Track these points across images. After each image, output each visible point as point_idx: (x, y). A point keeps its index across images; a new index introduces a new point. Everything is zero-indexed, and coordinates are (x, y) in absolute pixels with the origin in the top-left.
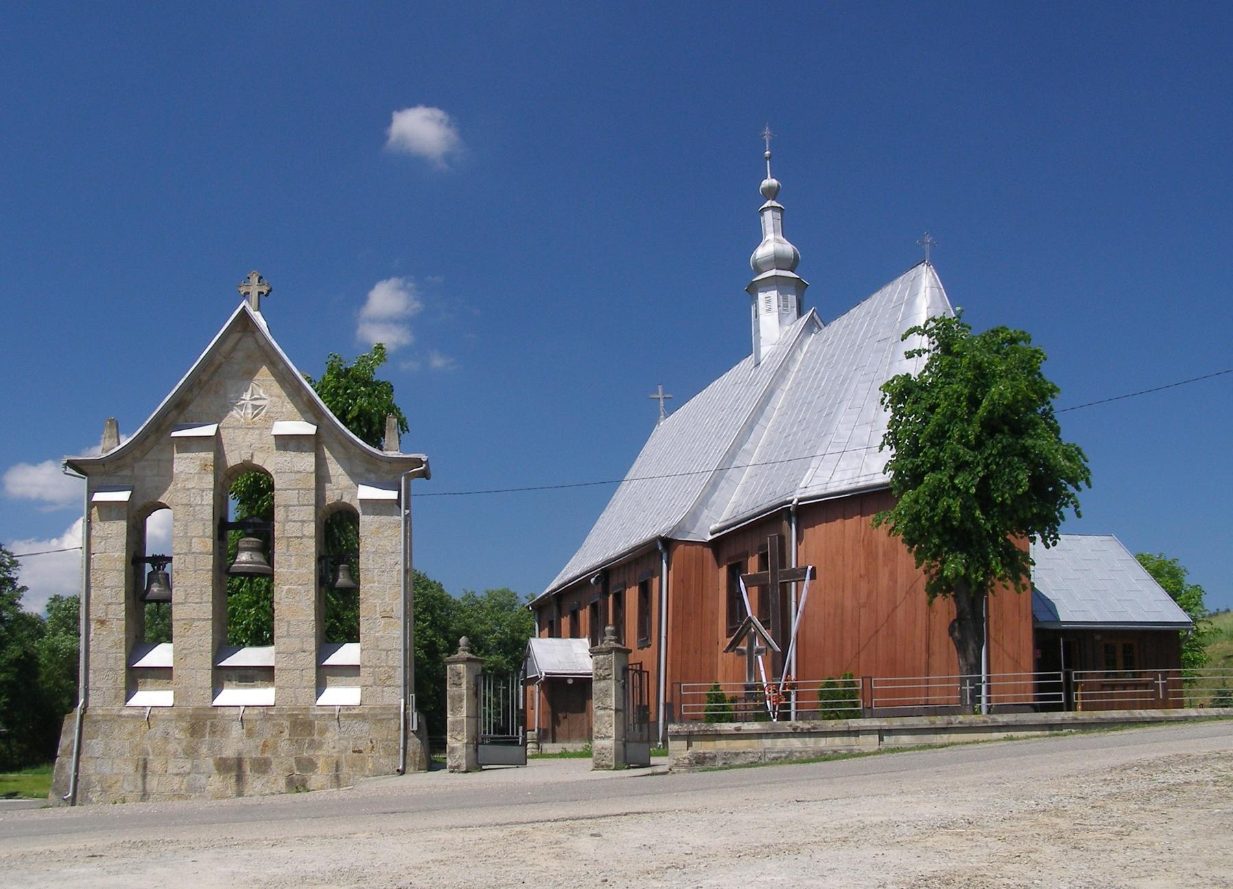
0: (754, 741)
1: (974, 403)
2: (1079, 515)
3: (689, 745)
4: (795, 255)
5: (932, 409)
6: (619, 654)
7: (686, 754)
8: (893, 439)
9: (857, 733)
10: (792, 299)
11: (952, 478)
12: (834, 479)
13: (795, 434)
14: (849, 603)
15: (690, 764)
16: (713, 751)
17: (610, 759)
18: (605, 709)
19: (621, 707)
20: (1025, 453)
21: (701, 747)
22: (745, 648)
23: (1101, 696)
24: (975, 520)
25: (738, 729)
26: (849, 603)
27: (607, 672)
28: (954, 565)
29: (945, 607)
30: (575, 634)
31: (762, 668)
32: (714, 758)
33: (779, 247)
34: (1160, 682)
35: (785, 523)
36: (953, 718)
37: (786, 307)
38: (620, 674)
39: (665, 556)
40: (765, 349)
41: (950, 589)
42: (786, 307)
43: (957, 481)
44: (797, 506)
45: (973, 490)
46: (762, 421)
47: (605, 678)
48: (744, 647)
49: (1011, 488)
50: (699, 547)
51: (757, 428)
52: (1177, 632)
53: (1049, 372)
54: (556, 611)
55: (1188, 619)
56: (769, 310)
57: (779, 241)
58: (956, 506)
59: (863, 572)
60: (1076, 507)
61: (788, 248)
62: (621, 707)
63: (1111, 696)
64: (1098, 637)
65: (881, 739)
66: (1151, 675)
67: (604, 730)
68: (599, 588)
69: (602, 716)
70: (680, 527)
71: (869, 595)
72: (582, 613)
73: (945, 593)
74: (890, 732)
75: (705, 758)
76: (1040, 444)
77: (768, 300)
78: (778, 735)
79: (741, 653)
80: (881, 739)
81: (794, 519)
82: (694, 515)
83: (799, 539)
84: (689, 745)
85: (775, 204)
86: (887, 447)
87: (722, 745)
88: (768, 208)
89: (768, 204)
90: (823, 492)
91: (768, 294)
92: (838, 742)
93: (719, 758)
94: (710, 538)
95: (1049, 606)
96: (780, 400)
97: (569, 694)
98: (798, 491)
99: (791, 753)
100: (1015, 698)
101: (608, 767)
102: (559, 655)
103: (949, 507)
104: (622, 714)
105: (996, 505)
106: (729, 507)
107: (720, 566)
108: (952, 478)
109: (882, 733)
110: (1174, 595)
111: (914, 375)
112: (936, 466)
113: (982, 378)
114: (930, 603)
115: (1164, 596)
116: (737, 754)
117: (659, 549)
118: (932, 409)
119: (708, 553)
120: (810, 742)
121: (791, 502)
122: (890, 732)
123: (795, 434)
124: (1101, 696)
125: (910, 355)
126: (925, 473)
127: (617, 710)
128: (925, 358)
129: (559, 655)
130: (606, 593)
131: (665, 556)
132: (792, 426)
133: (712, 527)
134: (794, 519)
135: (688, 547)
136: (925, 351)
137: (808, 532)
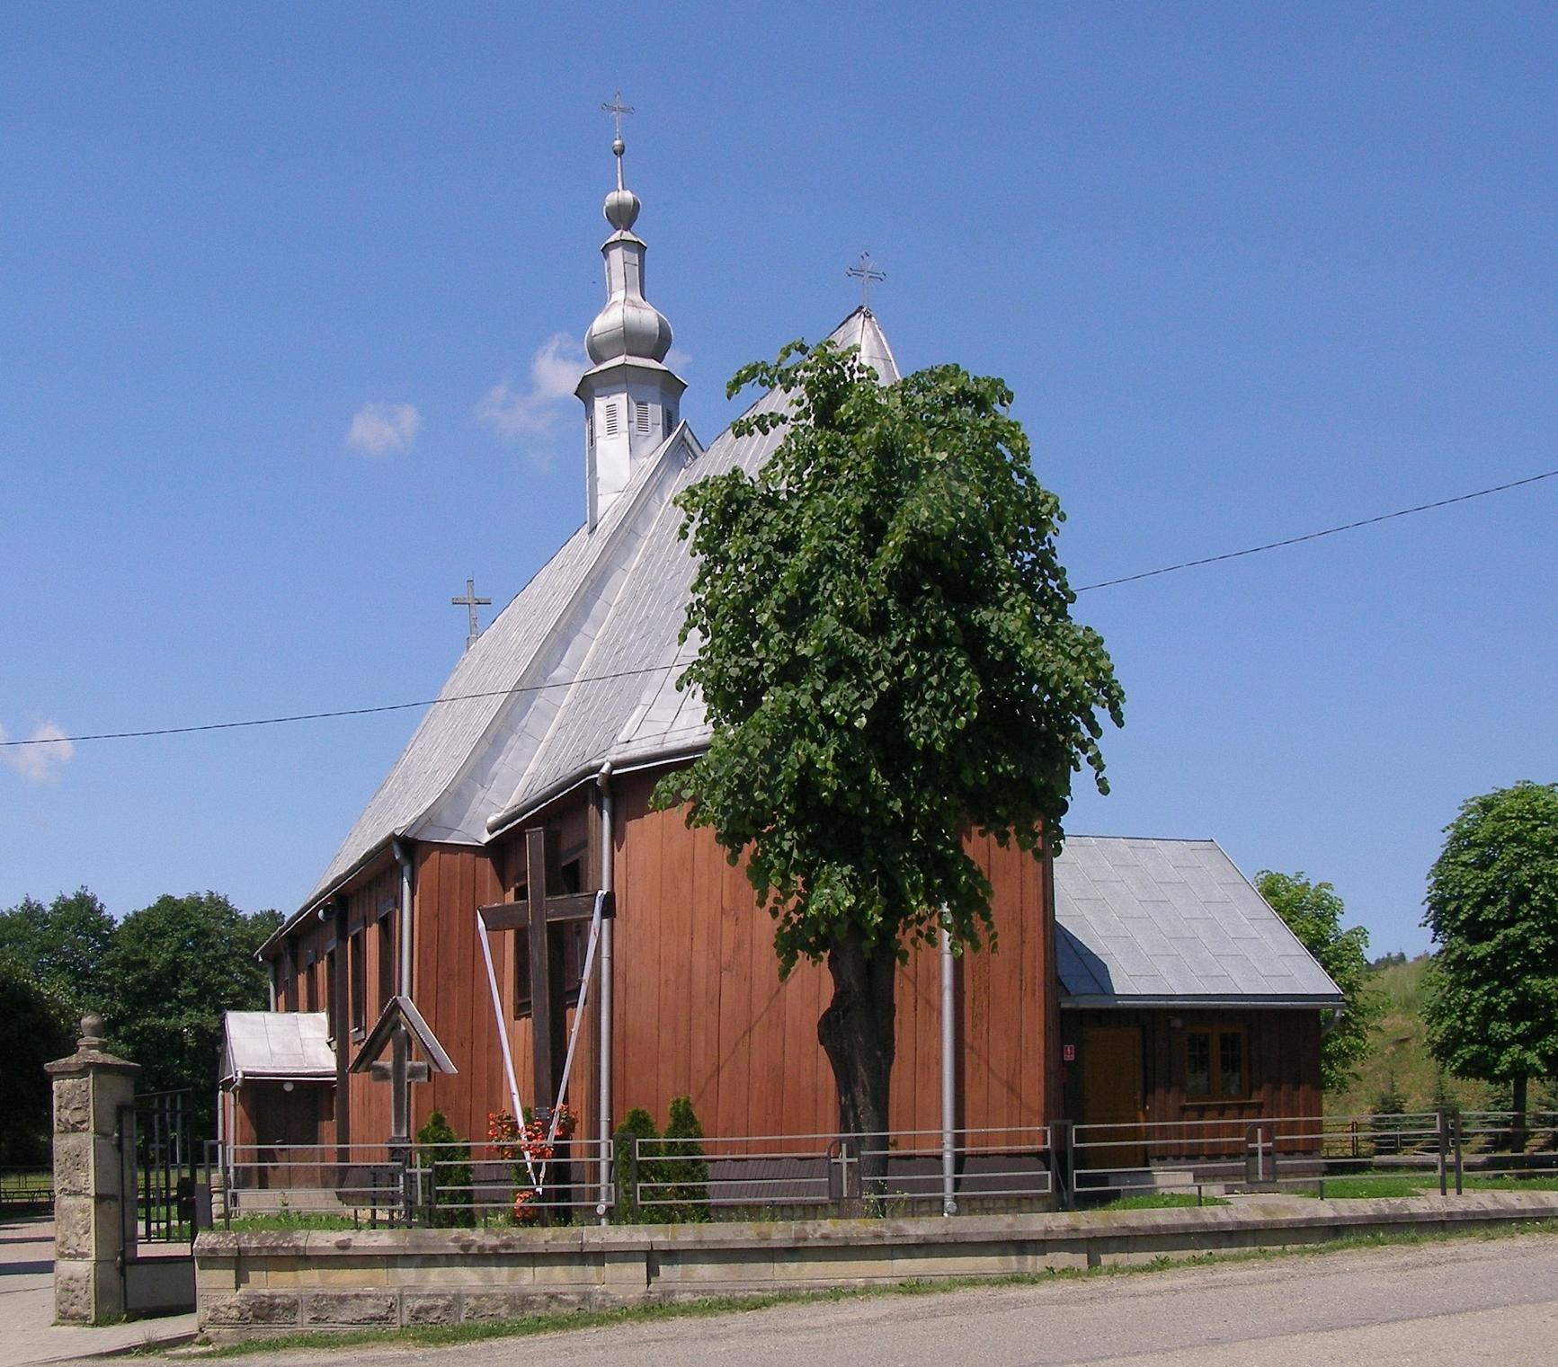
0: (380, 1273)
1: (873, 529)
2: (1105, 790)
3: (240, 1280)
4: (663, 326)
5: (788, 544)
6: (103, 1077)
7: (234, 1298)
8: (704, 614)
9: (598, 1257)
10: (655, 411)
11: (817, 696)
12: (675, 727)
13: (632, 644)
14: (701, 963)
15: (242, 1318)
16: (291, 1292)
17: (86, 1302)
18: (76, 1194)
19: (112, 1188)
20: (975, 639)
21: (265, 1283)
22: (389, 1064)
23: (1179, 1132)
24: (869, 794)
25: (343, 1246)
26: (701, 963)
27: (79, 1116)
28: (835, 892)
29: (814, 984)
30: (312, 1008)
31: (514, 1089)
32: (292, 1307)
33: (632, 314)
34: (1260, 1145)
35: (592, 809)
36: (809, 1226)
37: (642, 421)
38: (110, 1120)
39: (407, 869)
40: (606, 501)
41: (823, 943)
42: (642, 421)
43: (825, 702)
44: (609, 777)
45: (861, 722)
46: (586, 628)
47: (75, 1129)
48: (386, 1061)
49: (944, 717)
50: (470, 856)
51: (578, 639)
52: (1316, 1012)
53: (1050, 471)
54: (284, 958)
55: (1336, 990)
56: (612, 429)
57: (634, 305)
58: (825, 759)
59: (726, 904)
60: (1101, 768)
61: (648, 317)
62: (112, 1188)
63: (1197, 1132)
64: (1178, 1023)
65: (652, 1272)
66: (1236, 1129)
67: (73, 1241)
68: (333, 926)
69: (71, 1210)
70: (428, 818)
71: (738, 946)
72: (319, 966)
73: (814, 952)
74: (672, 1256)
75: (273, 1307)
76: (1006, 620)
77: (611, 411)
78: (430, 1260)
79: (382, 1074)
80: (652, 1272)
81: (606, 802)
82: (457, 796)
83: (617, 836)
84: (240, 1280)
85: (628, 236)
86: (695, 633)
87: (312, 1280)
88: (615, 244)
89: (616, 236)
90: (658, 750)
91: (613, 399)
92: (560, 1277)
93: (302, 1307)
94: (486, 838)
95: (1094, 970)
96: (620, 587)
97: (289, 1108)
98: (615, 749)
99: (458, 1298)
100: (1010, 1138)
101: (82, 1320)
102: (276, 1041)
103: (810, 762)
104: (114, 1207)
105: (916, 756)
106: (523, 782)
107: (505, 890)
108: (817, 696)
109: (654, 1258)
110: (1315, 946)
111: (751, 471)
112: (792, 672)
113: (892, 470)
114: (784, 974)
115: (1295, 947)
116: (342, 1300)
117: (404, 851)
118: (788, 544)
119: (486, 866)
120: (501, 1276)
121: (597, 769)
122: (672, 1256)
123: (632, 644)
124: (1179, 1132)
125: (741, 430)
126: (765, 687)
127: (100, 1198)
128: (778, 435)
129: (276, 1041)
130: (342, 937)
131: (407, 869)
132: (629, 631)
133: (491, 819)
134: (606, 802)
135: (446, 856)
136: (784, 419)
137: (633, 826)
